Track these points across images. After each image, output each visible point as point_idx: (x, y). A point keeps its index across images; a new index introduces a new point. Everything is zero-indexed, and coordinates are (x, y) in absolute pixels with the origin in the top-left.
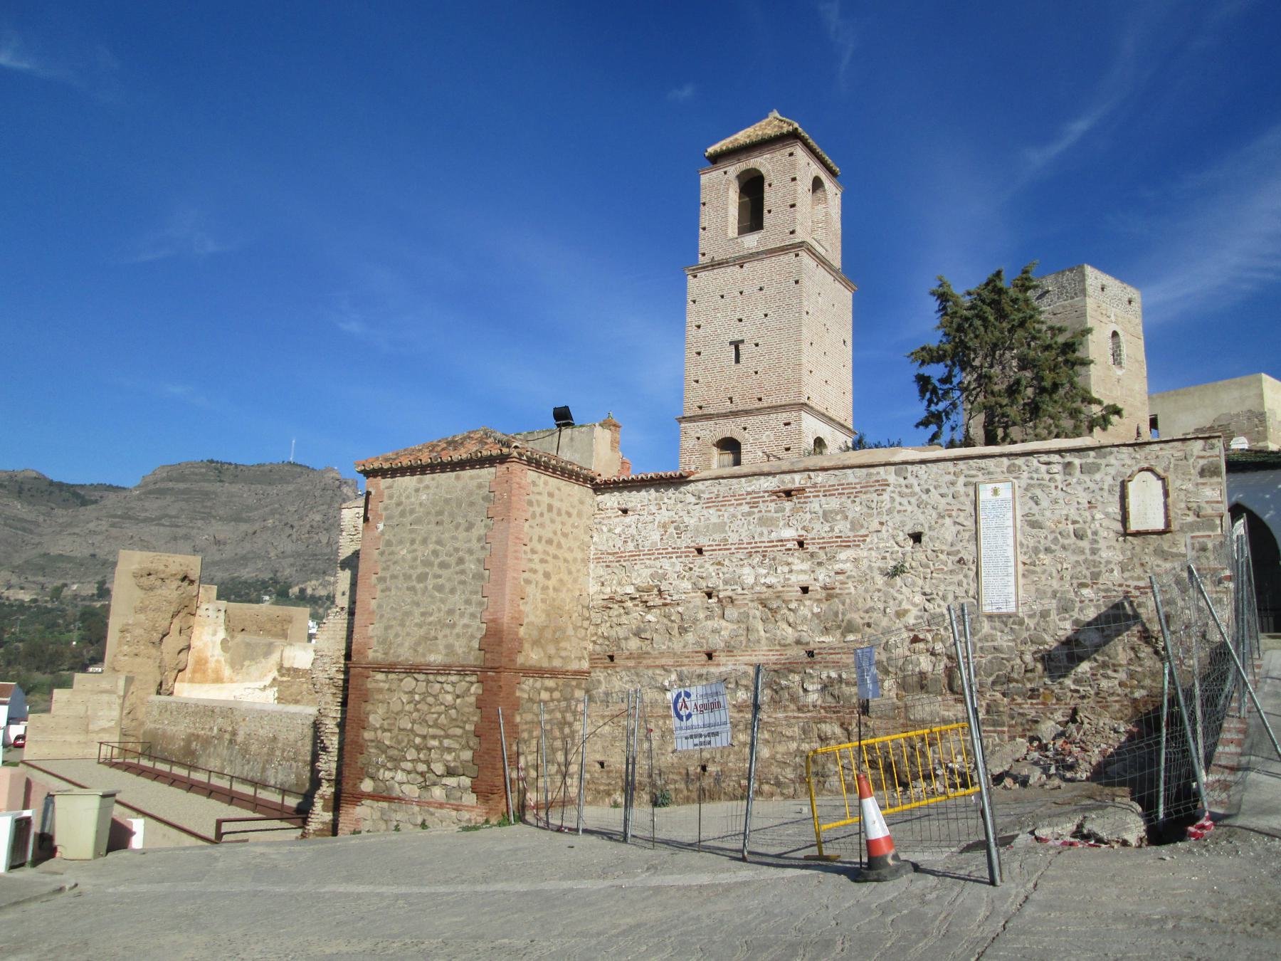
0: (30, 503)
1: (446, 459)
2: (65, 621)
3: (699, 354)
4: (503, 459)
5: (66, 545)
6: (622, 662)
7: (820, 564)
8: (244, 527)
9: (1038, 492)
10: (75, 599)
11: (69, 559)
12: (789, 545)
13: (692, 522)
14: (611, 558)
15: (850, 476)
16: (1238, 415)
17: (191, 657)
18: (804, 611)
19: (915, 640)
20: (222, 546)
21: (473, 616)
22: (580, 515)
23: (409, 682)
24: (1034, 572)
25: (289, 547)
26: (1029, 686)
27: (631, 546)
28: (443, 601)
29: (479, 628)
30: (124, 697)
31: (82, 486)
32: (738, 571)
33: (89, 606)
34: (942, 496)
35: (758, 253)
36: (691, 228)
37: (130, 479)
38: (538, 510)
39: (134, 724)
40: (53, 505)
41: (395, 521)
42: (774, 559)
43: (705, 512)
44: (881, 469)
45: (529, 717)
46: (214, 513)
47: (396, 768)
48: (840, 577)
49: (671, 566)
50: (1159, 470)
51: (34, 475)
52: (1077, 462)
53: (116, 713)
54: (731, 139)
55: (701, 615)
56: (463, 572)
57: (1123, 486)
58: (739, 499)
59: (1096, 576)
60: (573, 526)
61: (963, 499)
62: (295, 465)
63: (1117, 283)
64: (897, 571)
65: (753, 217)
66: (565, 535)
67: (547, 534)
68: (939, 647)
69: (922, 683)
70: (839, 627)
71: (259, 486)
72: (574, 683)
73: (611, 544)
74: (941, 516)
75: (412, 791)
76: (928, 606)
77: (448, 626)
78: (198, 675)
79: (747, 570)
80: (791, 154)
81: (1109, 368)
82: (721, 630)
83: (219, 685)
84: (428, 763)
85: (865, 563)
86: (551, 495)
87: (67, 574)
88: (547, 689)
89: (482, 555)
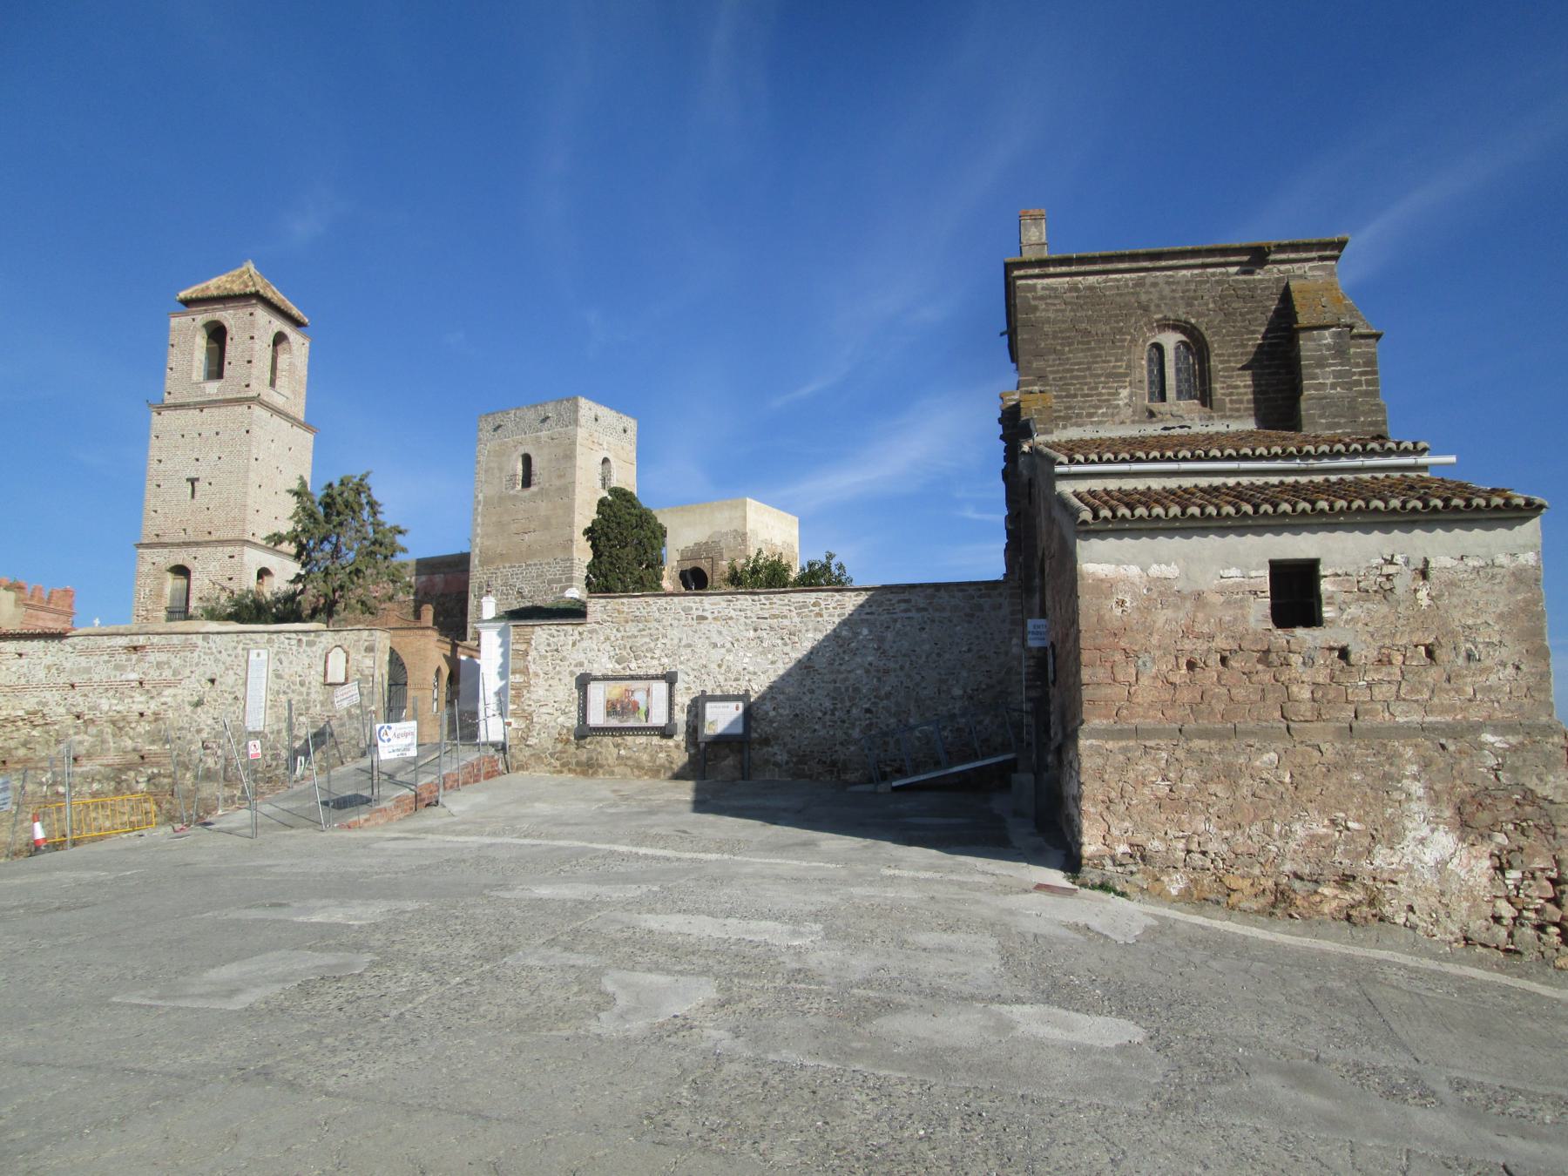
3: (159, 486)
6: (13, 766)
7: (152, 698)
9: (282, 656)
12: (133, 684)
13: (68, 665)
14: (7, 689)
15: (176, 639)
16: (727, 534)
19: (206, 748)
24: (275, 706)
26: (268, 775)
27: (23, 681)
32: (98, 701)
34: (229, 655)
35: (216, 401)
42: (123, 693)
43: (78, 658)
48: (164, 707)
49: (52, 697)
50: (345, 647)
54: (203, 285)
55: (71, 732)
57: (327, 656)
58: (102, 650)
59: (308, 709)
63: (613, 413)
64: (199, 703)
65: (216, 369)
70: (161, 739)
73: (8, 679)
74: (227, 669)
79: (104, 701)
80: (251, 314)
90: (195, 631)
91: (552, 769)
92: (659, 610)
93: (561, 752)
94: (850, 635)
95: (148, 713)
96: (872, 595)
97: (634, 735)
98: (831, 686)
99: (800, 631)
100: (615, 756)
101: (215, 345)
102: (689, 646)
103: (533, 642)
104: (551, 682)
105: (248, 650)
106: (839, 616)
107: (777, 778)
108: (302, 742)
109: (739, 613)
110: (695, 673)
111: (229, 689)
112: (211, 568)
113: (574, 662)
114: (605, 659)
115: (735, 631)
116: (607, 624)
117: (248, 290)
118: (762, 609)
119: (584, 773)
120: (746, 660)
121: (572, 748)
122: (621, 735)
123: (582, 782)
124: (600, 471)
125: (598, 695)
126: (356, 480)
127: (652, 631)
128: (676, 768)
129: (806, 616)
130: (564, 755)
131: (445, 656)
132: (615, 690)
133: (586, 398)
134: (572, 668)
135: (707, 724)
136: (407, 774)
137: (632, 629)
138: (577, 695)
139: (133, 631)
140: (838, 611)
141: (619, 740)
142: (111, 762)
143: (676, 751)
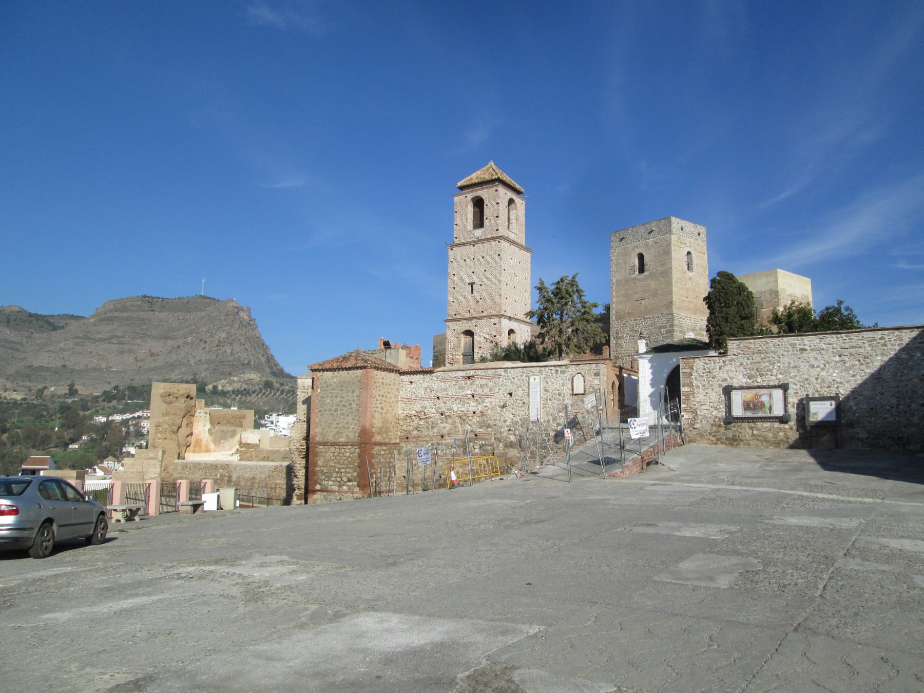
0: (16, 330)
1: (343, 366)
2: (48, 413)
3: (454, 288)
4: (365, 367)
5: (43, 360)
7: (479, 403)
8: (170, 343)
9: (548, 380)
10: (54, 397)
11: (48, 369)
13: (435, 387)
15: (490, 372)
16: (765, 292)
17: (193, 439)
18: (474, 420)
19: (510, 430)
20: (156, 357)
21: (355, 424)
22: (394, 384)
23: (332, 449)
24: (546, 407)
25: (204, 357)
27: (414, 396)
28: (344, 419)
29: (358, 429)
30: (162, 461)
31: (52, 316)
32: (452, 406)
33: (64, 402)
36: (450, 224)
37: (87, 310)
38: (378, 385)
39: (168, 475)
40: (33, 331)
41: (324, 389)
43: (440, 384)
44: (499, 370)
45: (377, 460)
46: (148, 333)
47: (329, 480)
48: (486, 408)
49: (428, 404)
50: (583, 373)
51: (17, 309)
52: (559, 370)
53: (158, 470)
54: (469, 178)
55: (439, 422)
56: (351, 408)
60: (392, 389)
61: (525, 381)
62: (205, 297)
63: (691, 224)
64: (504, 406)
65: (479, 221)
66: (389, 393)
67: (382, 393)
68: (517, 433)
69: (511, 445)
71: (180, 314)
72: (393, 448)
75: (335, 488)
76: (514, 418)
77: (347, 428)
78: (197, 449)
79: (455, 405)
80: (496, 191)
81: (684, 273)
82: (446, 427)
83: (209, 454)
84: (341, 478)
85: (494, 403)
86: (383, 378)
87: (46, 379)
88: (383, 450)
89: (358, 402)
90: (500, 367)
91: (711, 442)
92: (774, 346)
93: (715, 432)
94: (908, 357)
95: (477, 411)
96: (922, 331)
97: (762, 422)
98: (896, 390)
99: (871, 356)
100: (750, 434)
101: (478, 209)
102: (795, 367)
103: (694, 368)
104: (706, 391)
105: (529, 377)
106: (899, 345)
107: (860, 448)
108: (561, 427)
109: (828, 346)
110: (801, 384)
111: (520, 398)
112: (485, 331)
113: (721, 379)
114: (741, 377)
115: (826, 357)
116: (741, 355)
117: (494, 178)
118: (843, 343)
119: (731, 445)
120: (835, 375)
121: (722, 430)
122: (753, 422)
123: (734, 451)
124: (686, 259)
125: (738, 398)
126: (570, 278)
127: (770, 359)
128: (791, 442)
129: (875, 346)
130: (718, 434)
131: (616, 375)
132: (749, 395)
133: (675, 217)
134: (720, 382)
135: (811, 415)
136: (630, 445)
137: (757, 358)
138: (724, 398)
139: (467, 368)
140: (898, 342)
141: (753, 425)
142: (460, 438)
143: (791, 431)
